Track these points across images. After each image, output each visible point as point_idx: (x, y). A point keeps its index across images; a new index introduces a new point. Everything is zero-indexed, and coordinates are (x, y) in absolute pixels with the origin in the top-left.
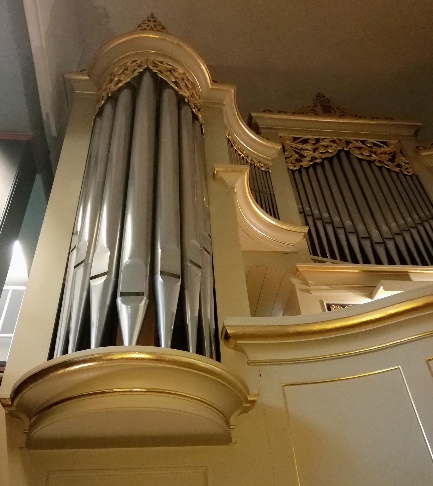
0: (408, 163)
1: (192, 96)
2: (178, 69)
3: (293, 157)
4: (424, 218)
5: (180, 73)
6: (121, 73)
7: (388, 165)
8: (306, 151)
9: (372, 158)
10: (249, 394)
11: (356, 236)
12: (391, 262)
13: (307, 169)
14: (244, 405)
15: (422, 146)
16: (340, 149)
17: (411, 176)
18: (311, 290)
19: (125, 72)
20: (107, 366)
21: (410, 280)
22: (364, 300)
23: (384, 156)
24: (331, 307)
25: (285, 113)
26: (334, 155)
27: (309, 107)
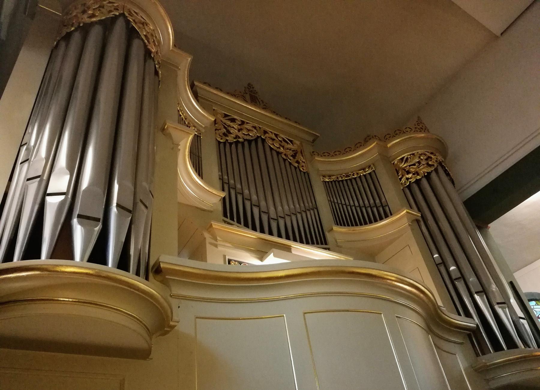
0: (304, 162)
1: (157, 53)
2: (150, 25)
3: (222, 130)
4: (307, 208)
5: (151, 29)
6: (96, 8)
7: (290, 159)
8: (233, 129)
9: (280, 150)
10: (172, 320)
11: (258, 209)
12: (280, 236)
13: (231, 144)
14: (165, 329)
15: (316, 152)
16: (259, 135)
17: (304, 173)
18: (218, 245)
19: (101, 9)
20: (70, 277)
21: (291, 252)
22: (255, 262)
23: (289, 152)
24: (231, 262)
25: (221, 90)
26: (254, 139)
27: (240, 92)
